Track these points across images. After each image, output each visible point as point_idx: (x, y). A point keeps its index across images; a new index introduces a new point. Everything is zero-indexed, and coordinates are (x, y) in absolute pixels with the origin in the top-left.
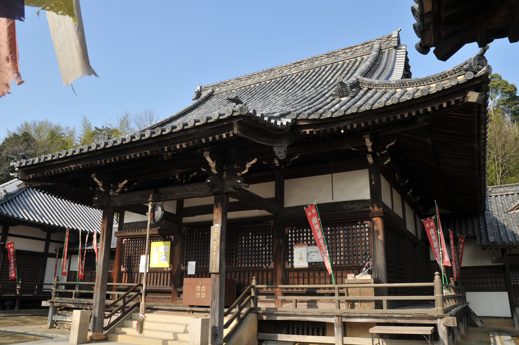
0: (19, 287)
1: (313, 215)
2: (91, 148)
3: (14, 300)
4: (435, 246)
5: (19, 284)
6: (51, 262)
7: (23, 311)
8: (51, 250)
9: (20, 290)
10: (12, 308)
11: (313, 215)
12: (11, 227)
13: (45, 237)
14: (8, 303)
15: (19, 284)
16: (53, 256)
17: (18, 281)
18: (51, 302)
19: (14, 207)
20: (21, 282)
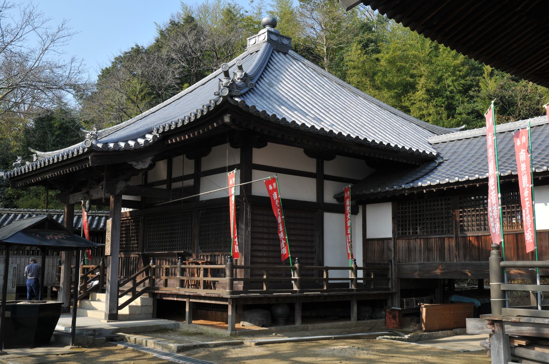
0: (296, 277)
1: (348, 198)
2: (210, 106)
3: (290, 303)
4: (529, 216)
5: (294, 269)
6: (332, 222)
7: (310, 326)
8: (329, 198)
9: (302, 284)
10: (289, 320)
11: (348, 198)
12: (255, 151)
13: (313, 170)
14: (280, 311)
15: (294, 269)
16: (332, 209)
17: (293, 264)
18: (493, 323)
19: (264, 101)
20: (300, 266)
